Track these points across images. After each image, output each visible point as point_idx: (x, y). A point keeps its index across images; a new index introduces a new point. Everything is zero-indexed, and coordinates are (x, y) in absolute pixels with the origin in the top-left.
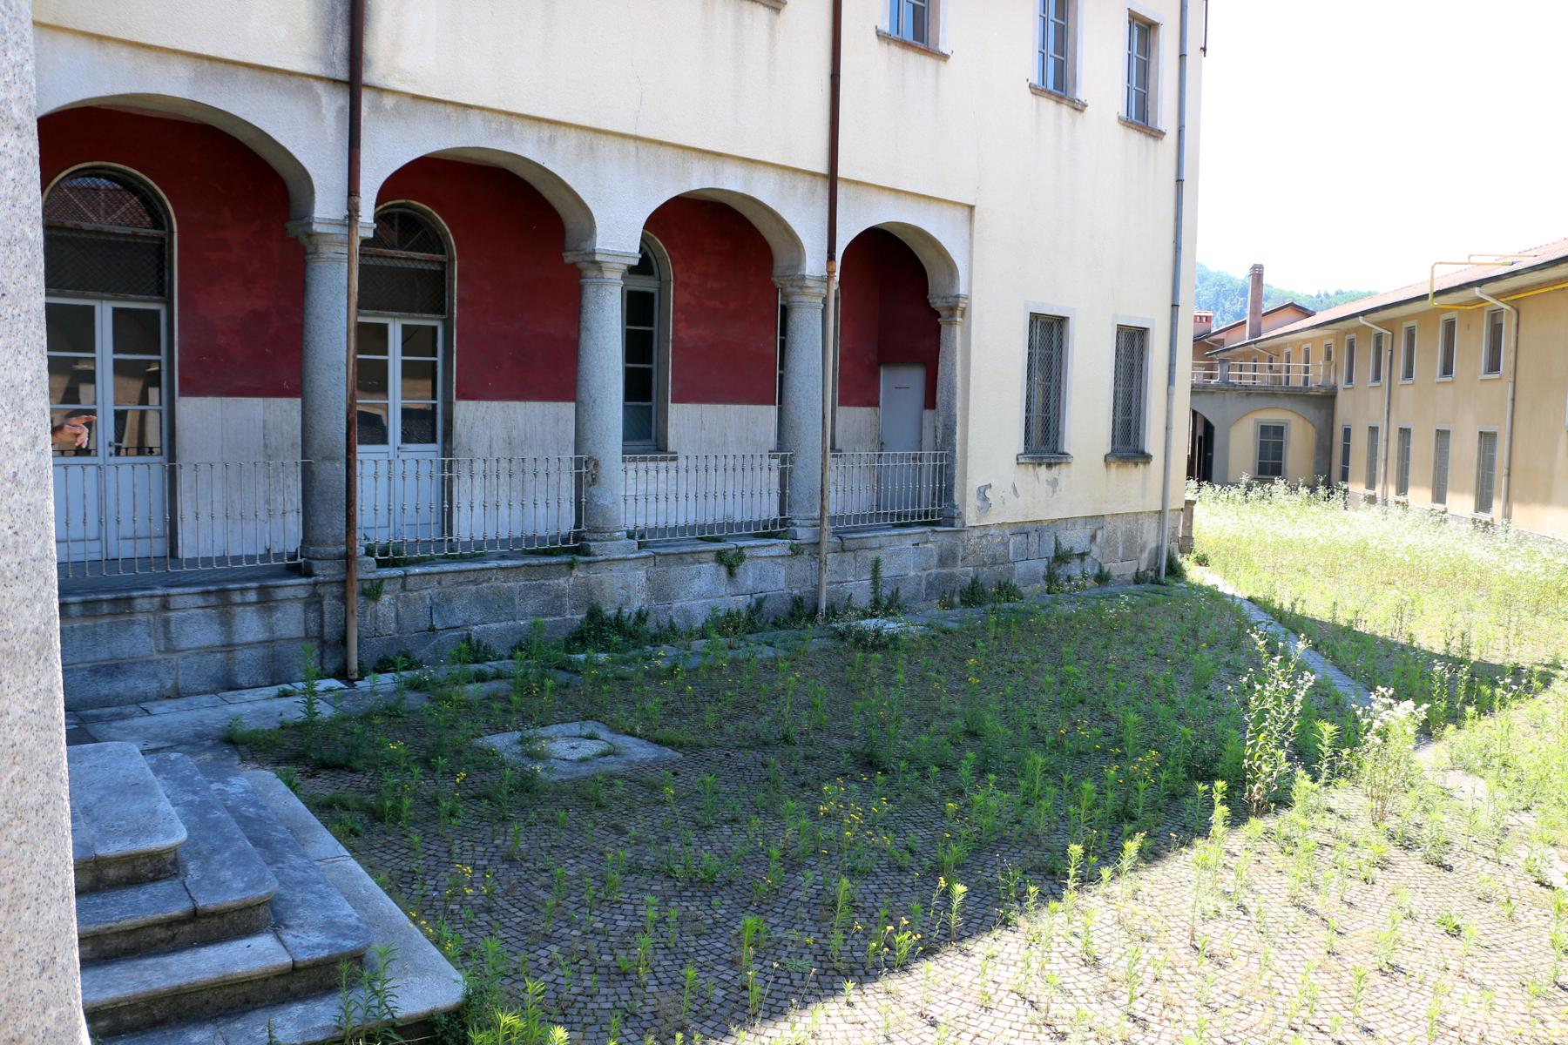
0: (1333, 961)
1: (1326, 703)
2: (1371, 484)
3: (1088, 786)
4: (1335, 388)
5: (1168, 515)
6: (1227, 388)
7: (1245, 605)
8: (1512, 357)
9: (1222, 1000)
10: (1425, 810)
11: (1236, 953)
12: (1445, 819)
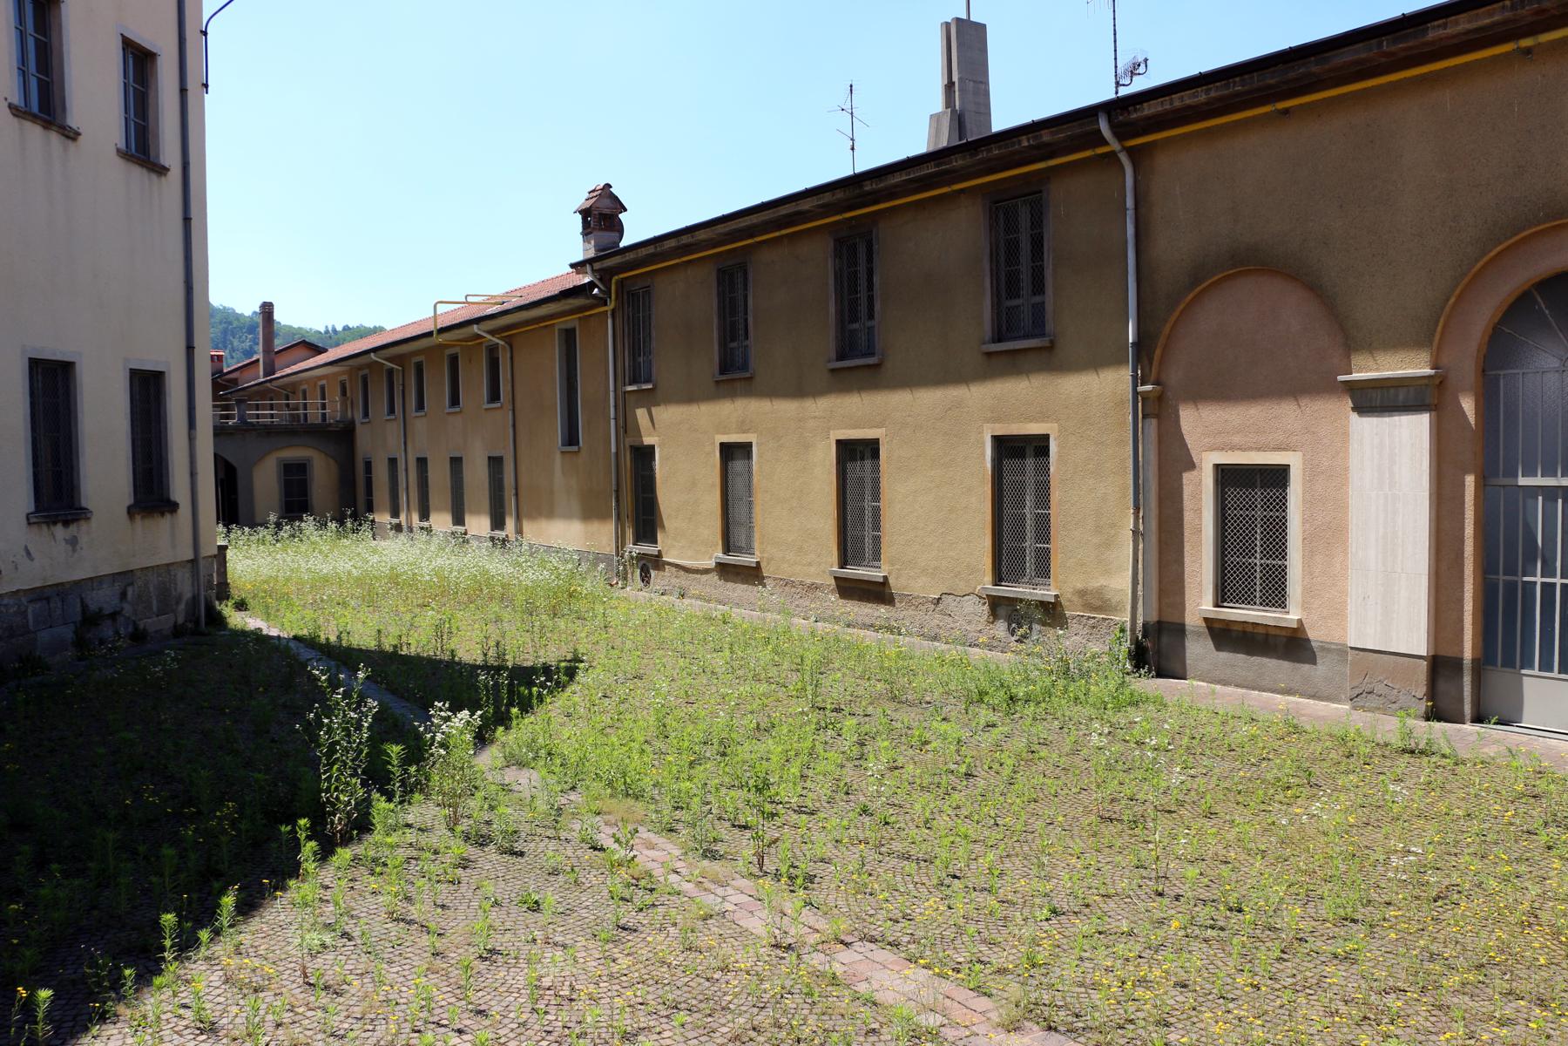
0: (438, 962)
1: (387, 727)
2: (395, 514)
3: (168, 851)
4: (352, 422)
5: (202, 563)
6: (245, 428)
7: (292, 644)
8: (509, 387)
9: (346, 1026)
10: (492, 808)
11: (350, 978)
12: (509, 811)
